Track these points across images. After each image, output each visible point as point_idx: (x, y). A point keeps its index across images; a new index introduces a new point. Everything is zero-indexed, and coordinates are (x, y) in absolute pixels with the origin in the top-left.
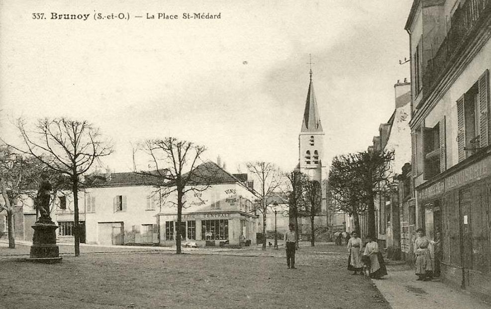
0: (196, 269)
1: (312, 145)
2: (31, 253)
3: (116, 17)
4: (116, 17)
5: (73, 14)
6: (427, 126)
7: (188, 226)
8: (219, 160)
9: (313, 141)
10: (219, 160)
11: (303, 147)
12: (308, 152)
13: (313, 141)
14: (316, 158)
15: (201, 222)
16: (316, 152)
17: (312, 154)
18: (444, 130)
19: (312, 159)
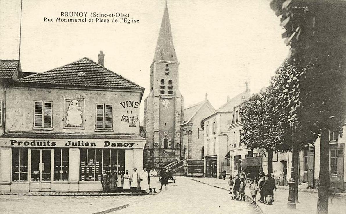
0: (68, 83)
1: (167, 74)
2: (319, 178)
3: (114, 15)
4: (114, 15)
5: (102, 14)
6: (70, 149)
7: (27, 174)
8: (101, 57)
9: (167, 70)
10: (101, 57)
11: (94, 107)
12: (162, 81)
13: (167, 70)
14: (170, 88)
15: (69, 177)
16: (170, 82)
17: (166, 84)
18: (133, 136)
19: (166, 90)
